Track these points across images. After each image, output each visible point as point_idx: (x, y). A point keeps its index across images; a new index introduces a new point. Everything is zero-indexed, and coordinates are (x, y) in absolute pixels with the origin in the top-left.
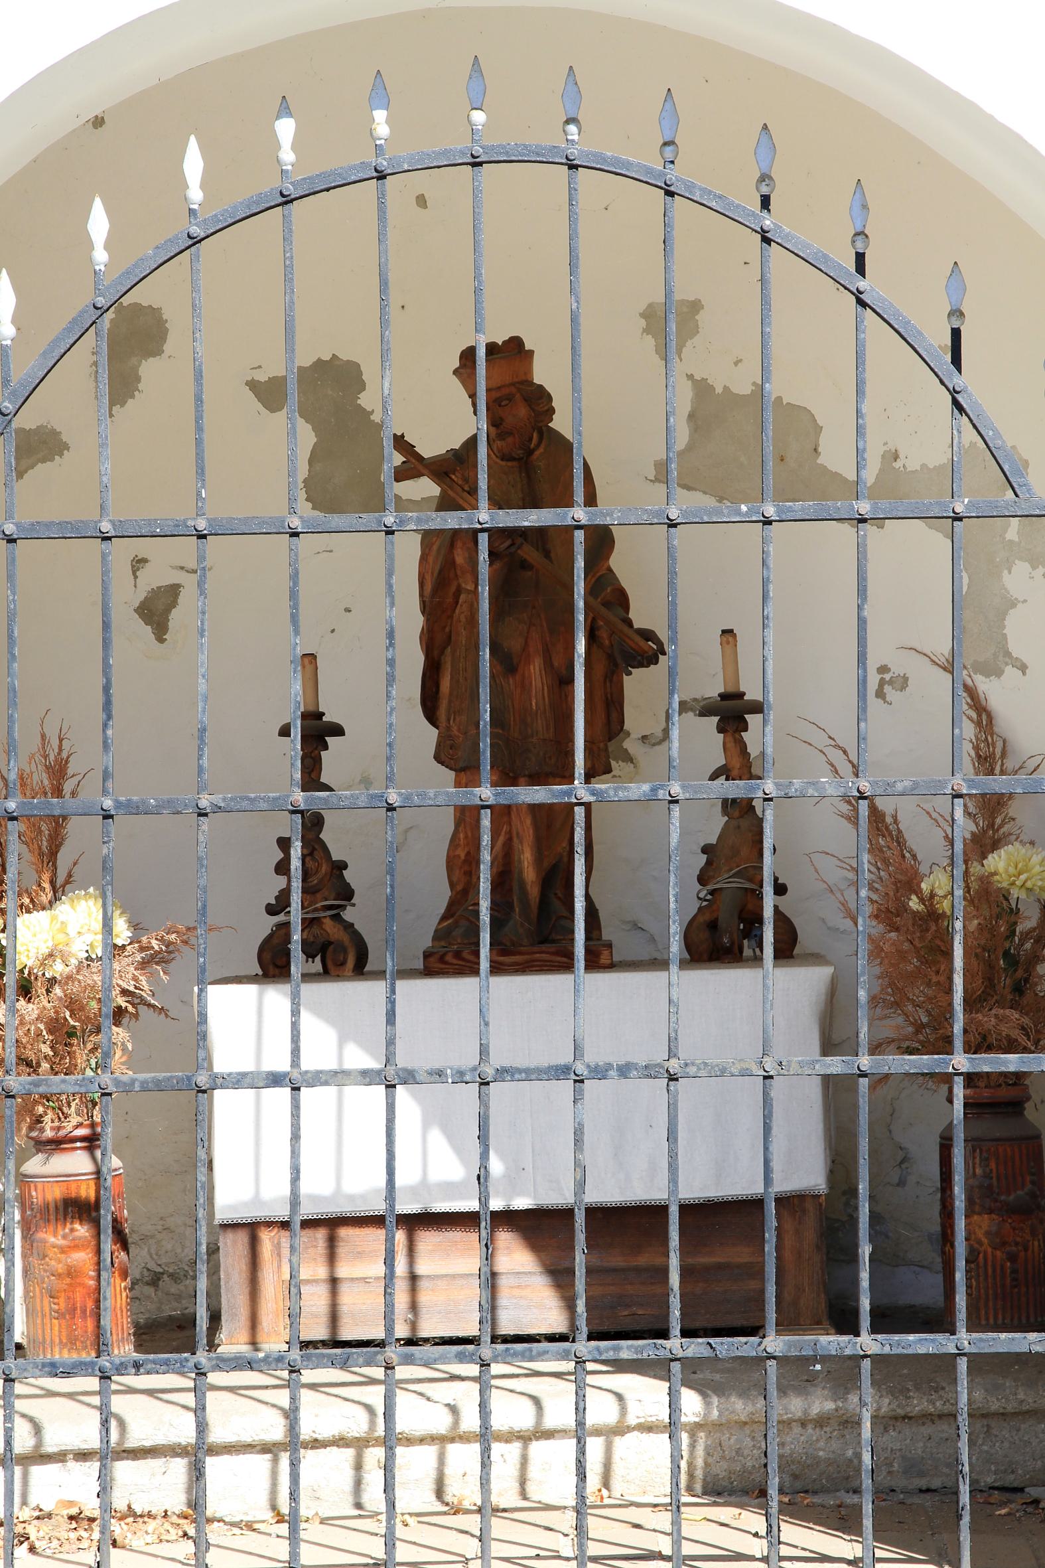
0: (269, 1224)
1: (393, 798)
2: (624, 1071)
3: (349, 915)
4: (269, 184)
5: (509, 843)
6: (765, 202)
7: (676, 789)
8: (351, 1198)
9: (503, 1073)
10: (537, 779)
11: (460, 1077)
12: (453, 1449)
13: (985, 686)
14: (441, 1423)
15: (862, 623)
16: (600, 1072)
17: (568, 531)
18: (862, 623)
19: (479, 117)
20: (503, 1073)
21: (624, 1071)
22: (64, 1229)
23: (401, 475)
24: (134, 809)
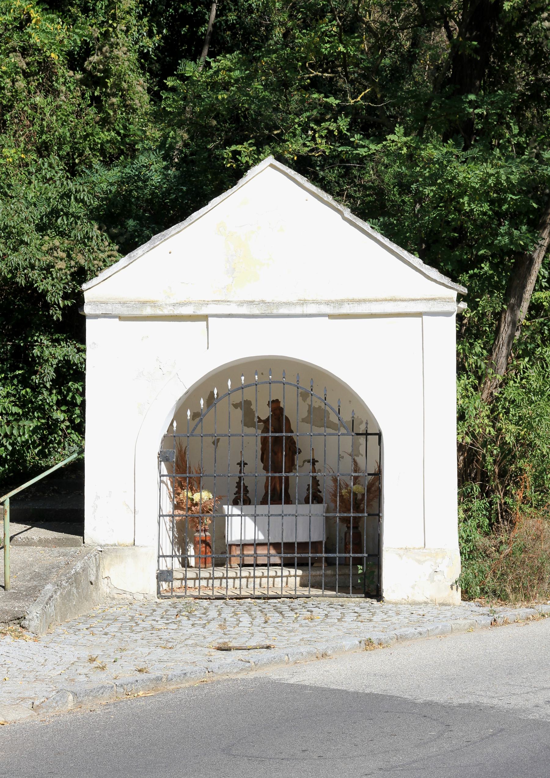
0: (234, 545)
1: (256, 475)
2: (289, 515)
3: (248, 495)
4: (240, 386)
5: (275, 484)
6: (312, 390)
7: (297, 474)
8: (248, 540)
9: (272, 515)
10: (279, 473)
11: (265, 515)
12: (263, 579)
13: (356, 458)
14: (261, 574)
15: (325, 450)
16: (286, 515)
17: (282, 436)
18: (325, 450)
19: (271, 377)
20: (272, 515)
21: (289, 515)
22: (452, 161)
23: (258, 422)
24: (219, 476)
